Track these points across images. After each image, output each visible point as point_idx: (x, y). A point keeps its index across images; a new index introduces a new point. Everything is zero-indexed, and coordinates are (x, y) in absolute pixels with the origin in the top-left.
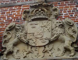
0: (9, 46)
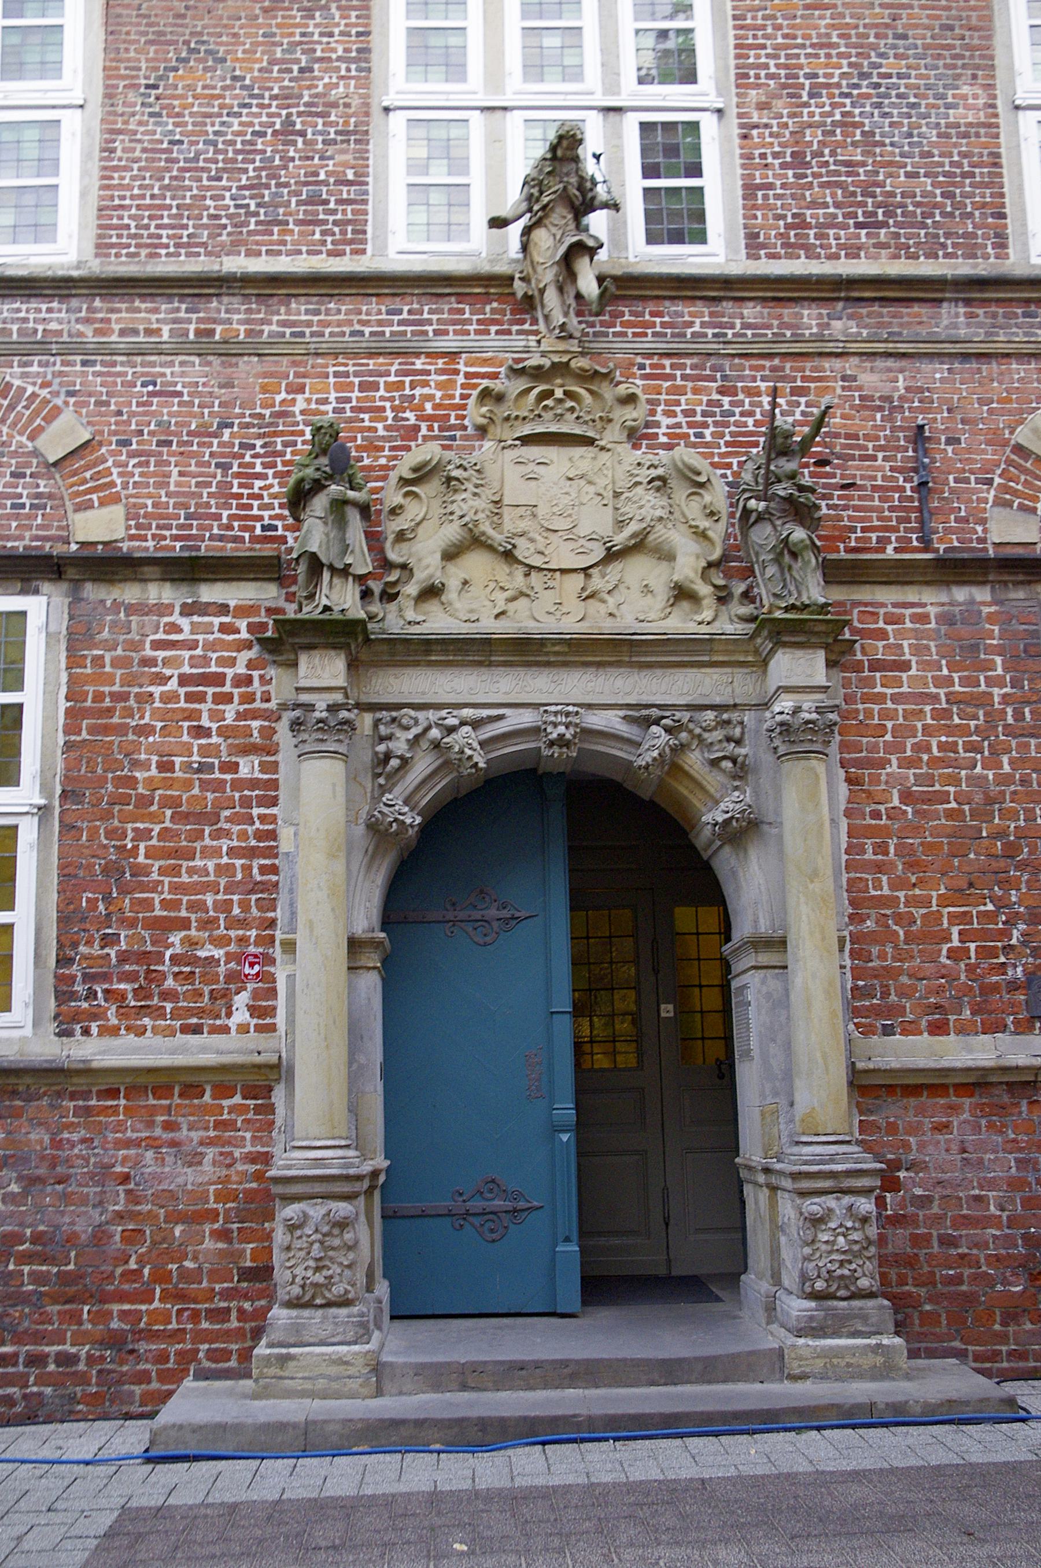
0: (425, 562)
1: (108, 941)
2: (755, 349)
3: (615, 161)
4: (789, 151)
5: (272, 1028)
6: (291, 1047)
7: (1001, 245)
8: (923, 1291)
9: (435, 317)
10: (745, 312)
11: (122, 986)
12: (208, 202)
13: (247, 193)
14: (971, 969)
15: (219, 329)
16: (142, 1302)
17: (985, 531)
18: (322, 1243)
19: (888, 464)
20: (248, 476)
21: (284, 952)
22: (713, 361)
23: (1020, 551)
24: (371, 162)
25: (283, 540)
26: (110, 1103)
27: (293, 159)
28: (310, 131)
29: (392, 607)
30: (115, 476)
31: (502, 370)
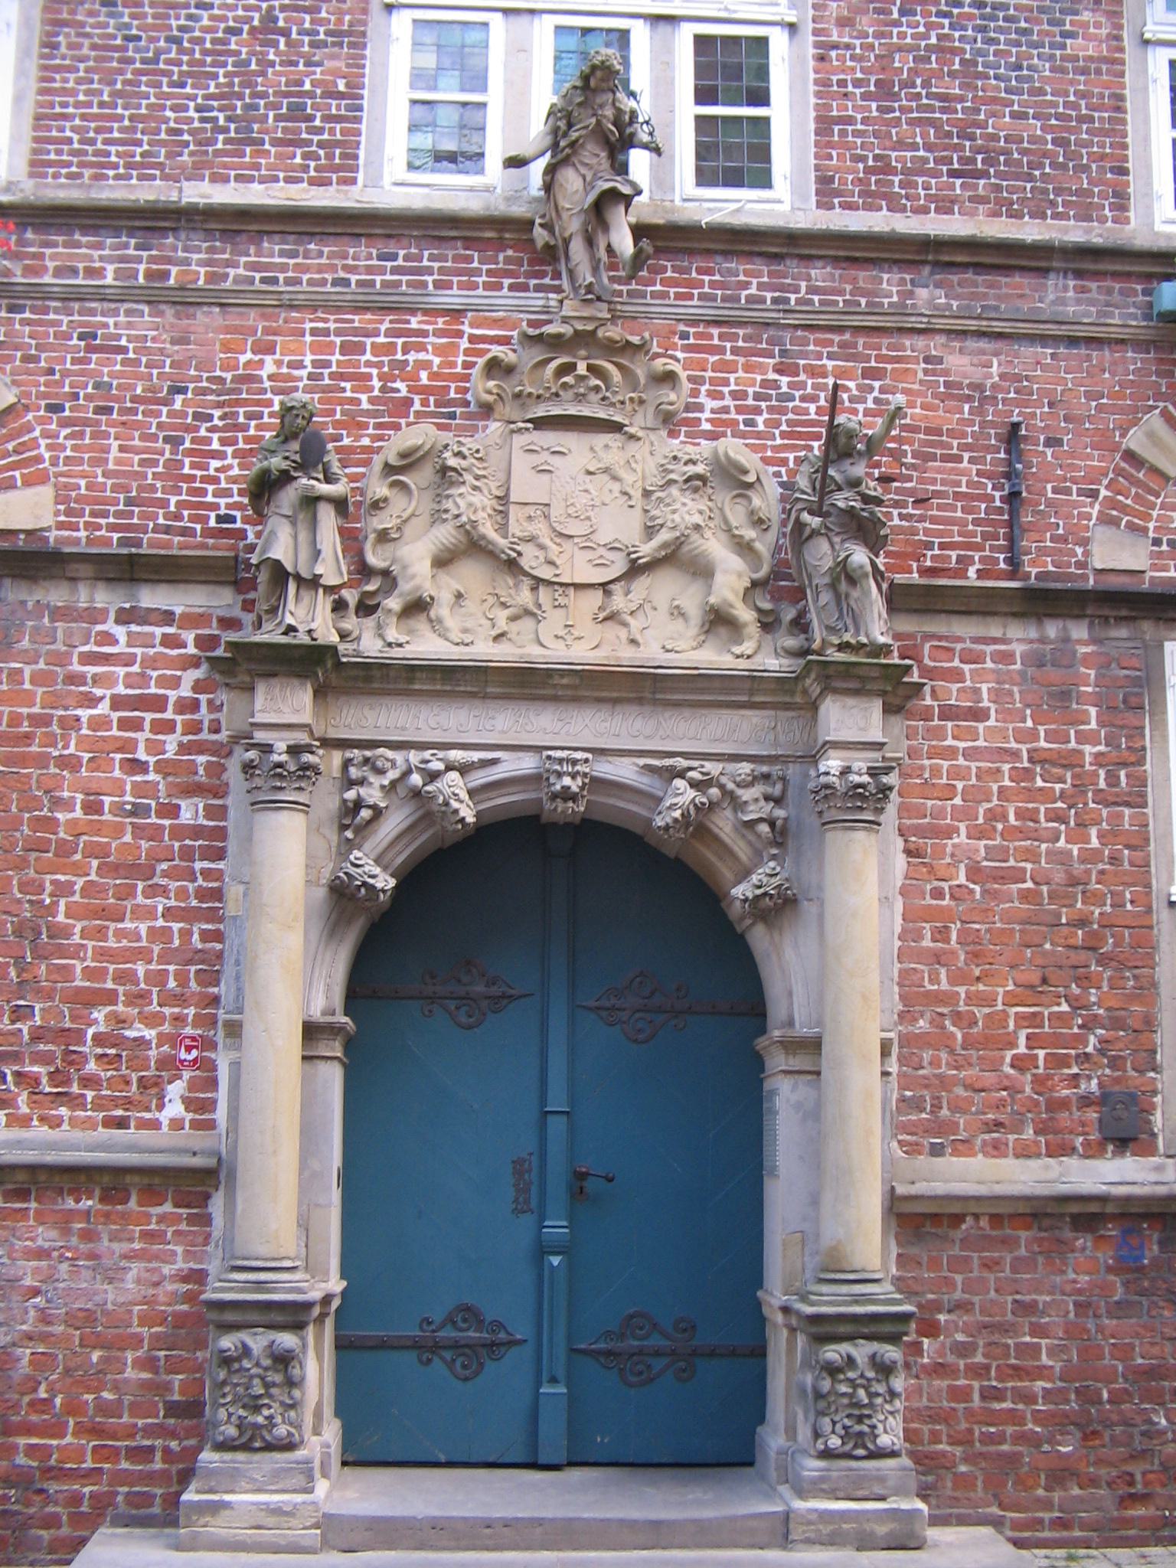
2: (822, 320)
3: (663, 89)
5: (211, 1125)
6: (234, 1149)
7: (1121, 203)
8: (958, 1451)
9: (436, 265)
10: (813, 272)
11: (35, 1069)
12: (169, 113)
13: (215, 104)
14: (1037, 1080)
16: (53, 1436)
17: (1086, 554)
18: (263, 1379)
19: (974, 467)
21: (228, 1035)
22: (772, 332)
24: (367, 71)
25: (242, 534)
27: (272, 64)
28: (294, 29)
29: (370, 622)
30: (42, 449)
31: (515, 333)
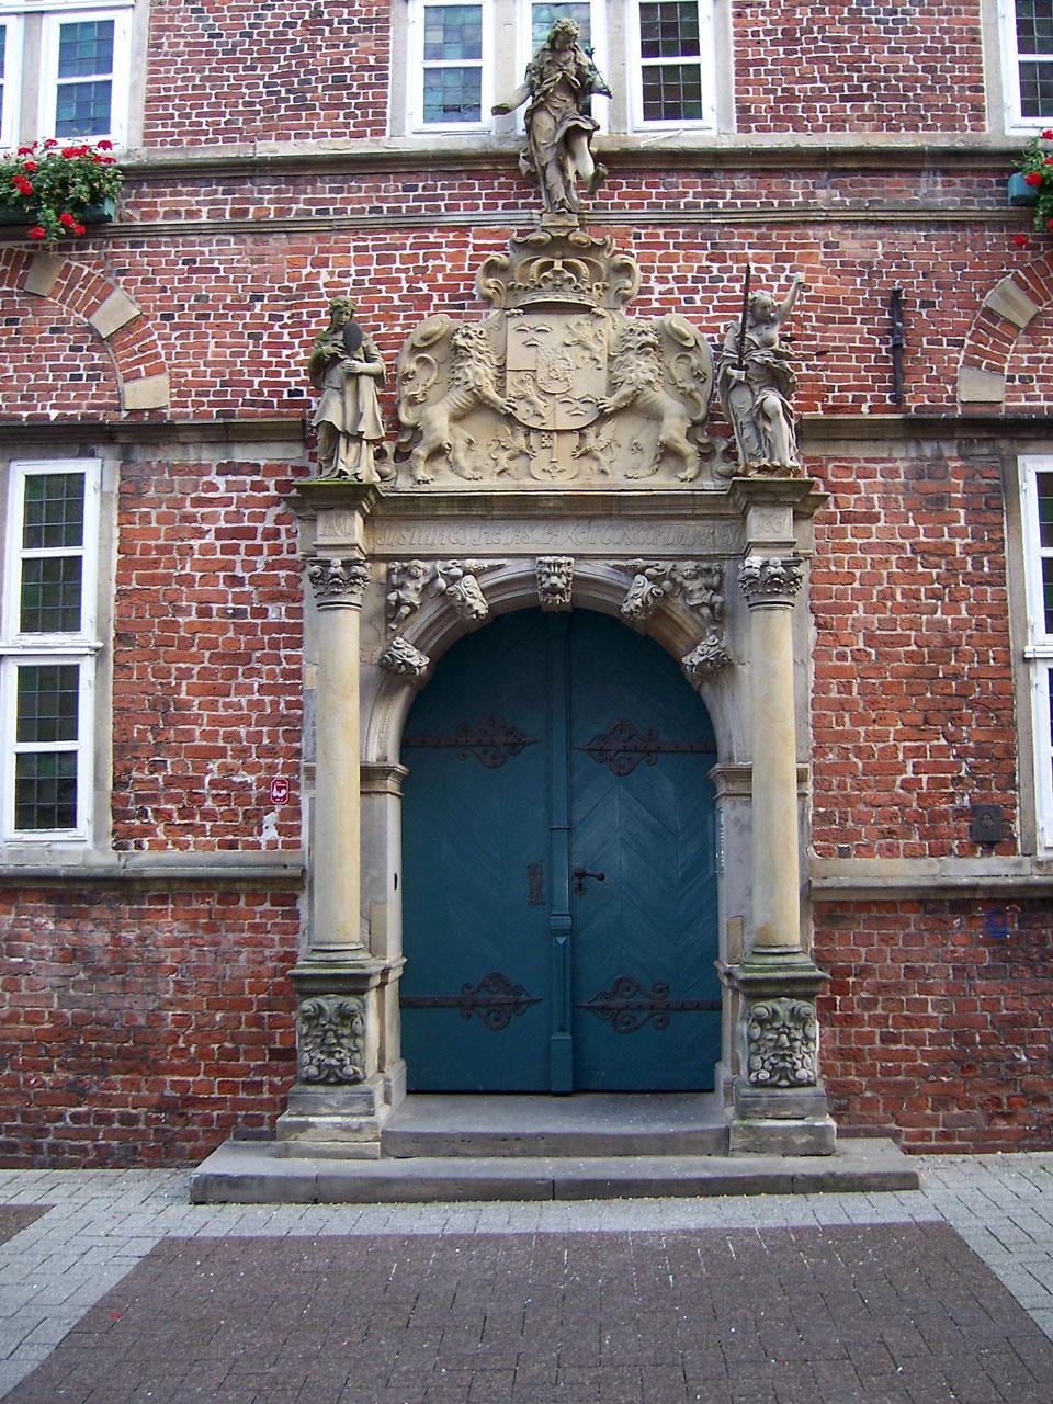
1: (157, 767)
4: (780, 29)
5: (297, 845)
9: (446, 192)
11: (169, 807)
12: (244, 90)
15: (252, 208)
16: (191, 1075)
17: (955, 390)
20: (277, 346)
23: (986, 410)
25: (308, 404)
26: (159, 907)
30: (159, 348)
